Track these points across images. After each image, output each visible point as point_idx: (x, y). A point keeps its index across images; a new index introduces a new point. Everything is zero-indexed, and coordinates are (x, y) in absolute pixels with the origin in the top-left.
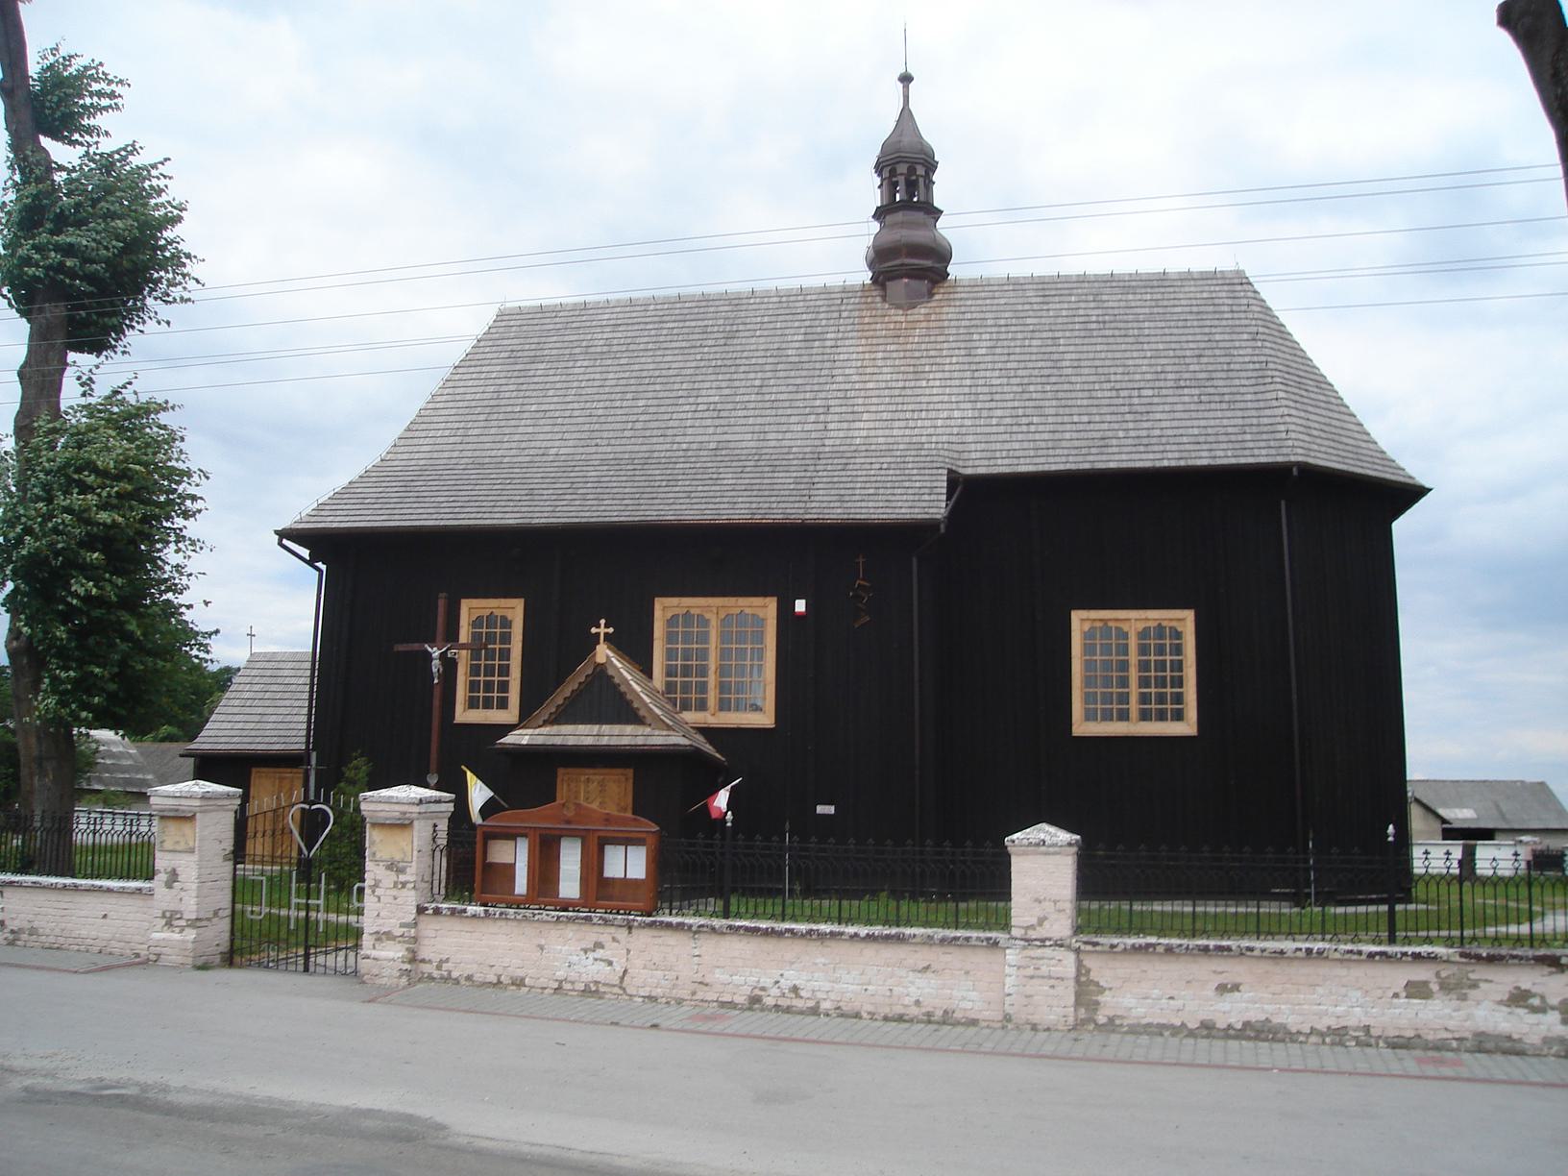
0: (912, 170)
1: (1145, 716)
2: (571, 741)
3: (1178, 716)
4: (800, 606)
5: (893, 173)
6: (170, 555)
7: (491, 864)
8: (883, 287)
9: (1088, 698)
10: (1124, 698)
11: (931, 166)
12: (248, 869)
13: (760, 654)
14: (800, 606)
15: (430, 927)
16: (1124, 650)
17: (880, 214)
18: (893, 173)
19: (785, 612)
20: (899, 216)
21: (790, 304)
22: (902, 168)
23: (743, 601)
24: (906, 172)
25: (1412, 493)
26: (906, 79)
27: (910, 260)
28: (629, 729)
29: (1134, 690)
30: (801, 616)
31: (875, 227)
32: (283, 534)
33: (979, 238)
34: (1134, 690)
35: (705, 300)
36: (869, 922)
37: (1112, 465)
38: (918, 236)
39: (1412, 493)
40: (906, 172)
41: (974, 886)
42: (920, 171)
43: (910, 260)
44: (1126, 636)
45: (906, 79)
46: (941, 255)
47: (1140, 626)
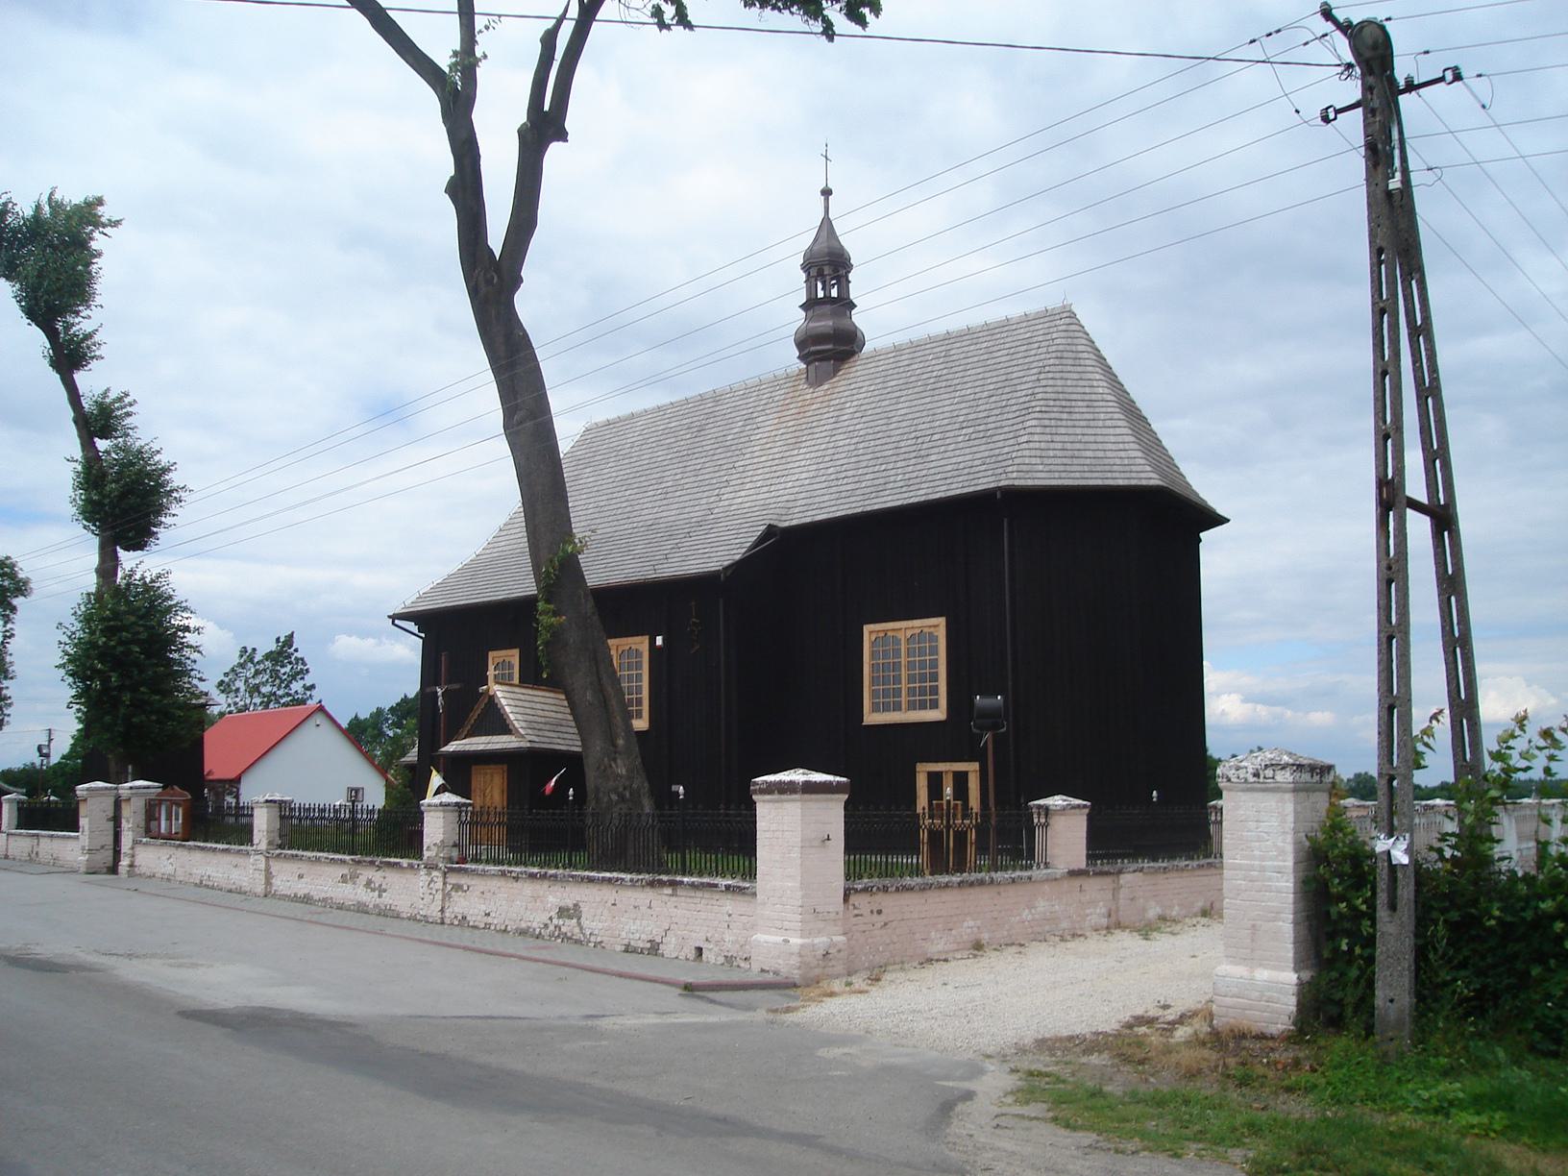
1: (912, 706)
2: (473, 748)
4: (659, 641)
6: (8, 659)
9: (874, 694)
10: (897, 693)
14: (659, 641)
15: (139, 849)
16: (897, 653)
17: (805, 307)
19: (652, 642)
21: (775, 382)
23: (630, 640)
24: (828, 265)
26: (827, 193)
27: (830, 344)
28: (505, 738)
29: (904, 686)
33: (880, 314)
34: (904, 686)
35: (915, 347)
36: (700, 874)
37: (1121, 482)
40: (828, 265)
41: (723, 844)
43: (830, 344)
44: (899, 642)
45: (827, 193)
47: (909, 633)
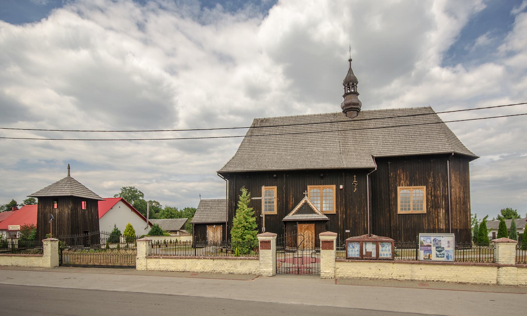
0: (353, 84)
3: (402, 209)
4: (341, 187)
5: (348, 85)
7: (206, 229)
8: (346, 113)
11: (357, 83)
12: (84, 205)
13: (402, 202)
17: (344, 96)
18: (348, 85)
19: (338, 189)
20: (348, 96)
22: (351, 83)
25: (473, 158)
30: (342, 189)
31: (343, 99)
32: (220, 173)
38: (354, 101)
39: (473, 158)
42: (355, 84)
46: (358, 104)
